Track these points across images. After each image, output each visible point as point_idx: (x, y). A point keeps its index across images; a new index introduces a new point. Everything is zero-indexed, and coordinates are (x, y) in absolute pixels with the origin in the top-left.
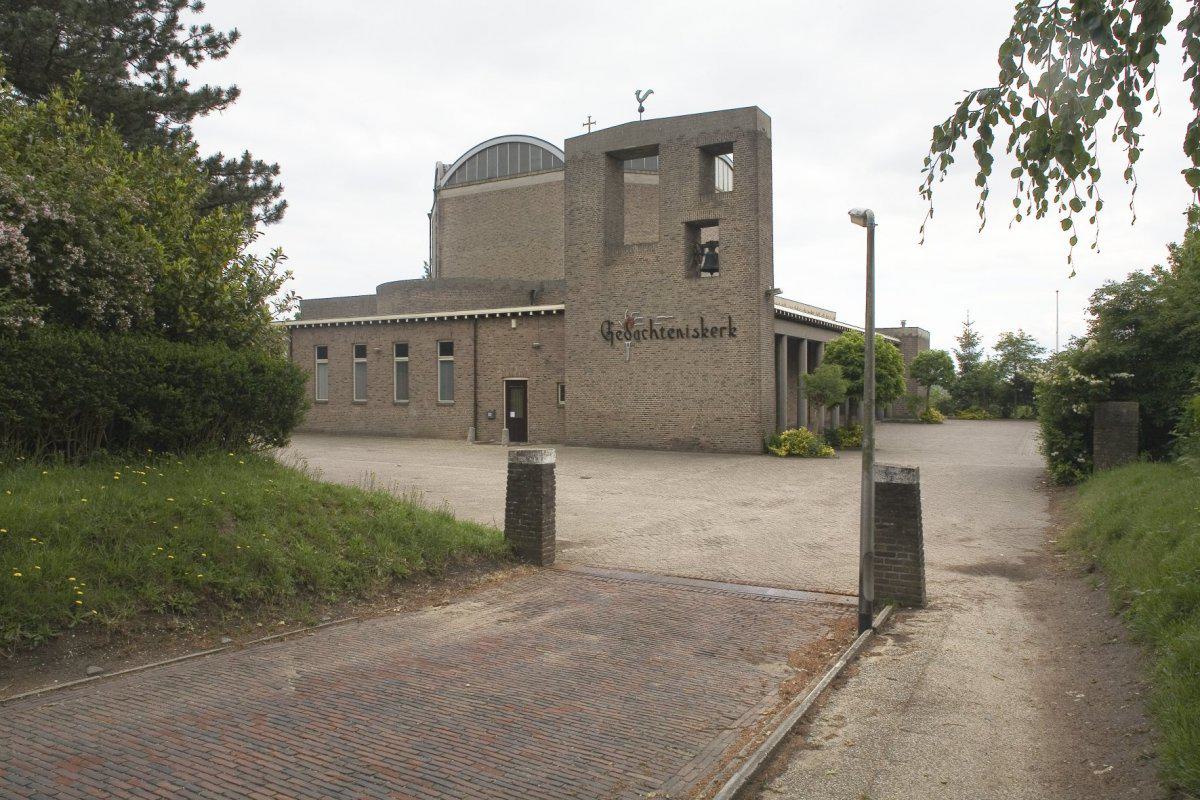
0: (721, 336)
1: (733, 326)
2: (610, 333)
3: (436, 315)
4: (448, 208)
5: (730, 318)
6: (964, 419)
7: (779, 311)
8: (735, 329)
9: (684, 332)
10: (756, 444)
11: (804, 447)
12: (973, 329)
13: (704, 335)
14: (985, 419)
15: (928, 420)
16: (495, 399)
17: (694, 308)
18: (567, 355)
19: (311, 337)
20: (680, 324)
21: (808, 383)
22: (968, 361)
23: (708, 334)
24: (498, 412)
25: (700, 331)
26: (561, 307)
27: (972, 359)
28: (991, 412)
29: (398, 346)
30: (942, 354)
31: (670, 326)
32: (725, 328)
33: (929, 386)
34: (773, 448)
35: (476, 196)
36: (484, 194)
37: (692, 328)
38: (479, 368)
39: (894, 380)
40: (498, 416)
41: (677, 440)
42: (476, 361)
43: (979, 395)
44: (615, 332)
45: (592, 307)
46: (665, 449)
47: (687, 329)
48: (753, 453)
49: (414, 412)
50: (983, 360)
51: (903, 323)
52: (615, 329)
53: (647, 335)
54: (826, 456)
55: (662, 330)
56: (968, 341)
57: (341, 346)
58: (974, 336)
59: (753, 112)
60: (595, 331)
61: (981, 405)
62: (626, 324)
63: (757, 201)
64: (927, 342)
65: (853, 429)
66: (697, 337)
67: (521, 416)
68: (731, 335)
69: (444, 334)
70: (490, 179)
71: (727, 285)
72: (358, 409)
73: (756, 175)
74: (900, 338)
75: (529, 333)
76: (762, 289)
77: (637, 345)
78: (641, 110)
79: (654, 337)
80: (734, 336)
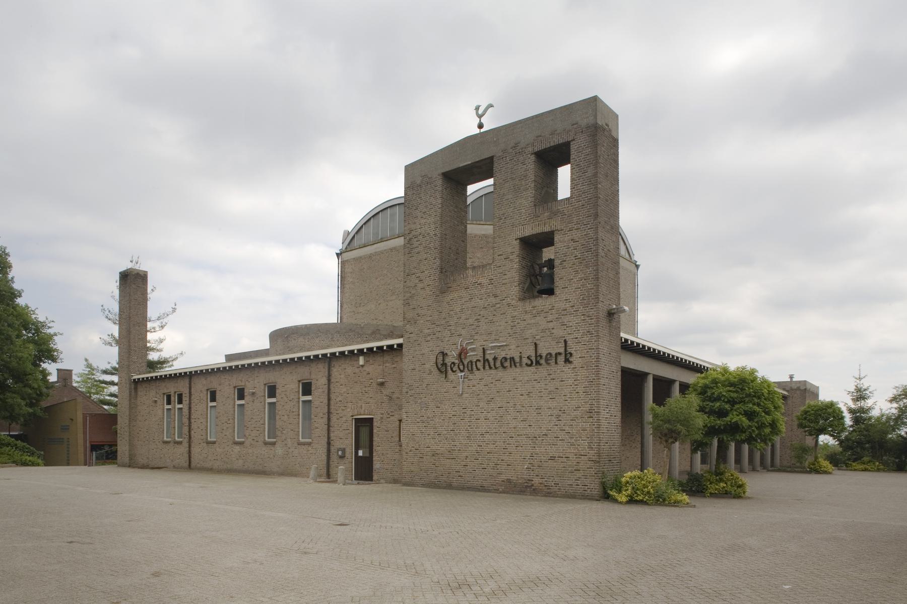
0: (556, 363)
1: (569, 350)
2: (444, 364)
3: (295, 356)
4: (348, 269)
5: (565, 342)
6: (855, 470)
7: (626, 340)
8: (571, 354)
9: (517, 360)
10: (595, 488)
11: (648, 492)
12: (865, 384)
13: (538, 363)
14: (878, 470)
15: (815, 470)
16: (345, 438)
17: (528, 333)
18: (405, 390)
19: (205, 382)
20: (513, 352)
21: (656, 416)
22: (859, 416)
23: (543, 361)
24: (348, 451)
25: (533, 358)
26: (400, 341)
27: (864, 413)
28: (885, 464)
29: (269, 387)
30: (832, 405)
31: (503, 354)
32: (560, 354)
33: (817, 436)
34: (613, 493)
35: (370, 256)
36: (376, 254)
37: (525, 355)
38: (332, 407)
39: (769, 418)
40: (347, 455)
41: (509, 481)
42: (329, 400)
43: (872, 448)
44: (449, 364)
45: (429, 338)
46: (497, 491)
47: (521, 357)
48: (590, 498)
49: (279, 450)
50: (875, 413)
51: (791, 377)
52: (448, 361)
53: (480, 365)
54: (676, 504)
55: (495, 359)
56: (860, 395)
57: (226, 389)
58: (865, 390)
59: (594, 101)
60: (430, 365)
61: (873, 457)
62: (460, 355)
63: (596, 205)
64: (816, 395)
65: (722, 474)
66: (531, 365)
67: (367, 455)
68: (567, 361)
69: (303, 373)
70: (382, 241)
71: (562, 305)
72: (237, 448)
73: (595, 175)
74: (787, 391)
75: (374, 369)
76: (603, 307)
77: (471, 377)
78: (480, 126)
79: (487, 367)
80: (570, 362)
